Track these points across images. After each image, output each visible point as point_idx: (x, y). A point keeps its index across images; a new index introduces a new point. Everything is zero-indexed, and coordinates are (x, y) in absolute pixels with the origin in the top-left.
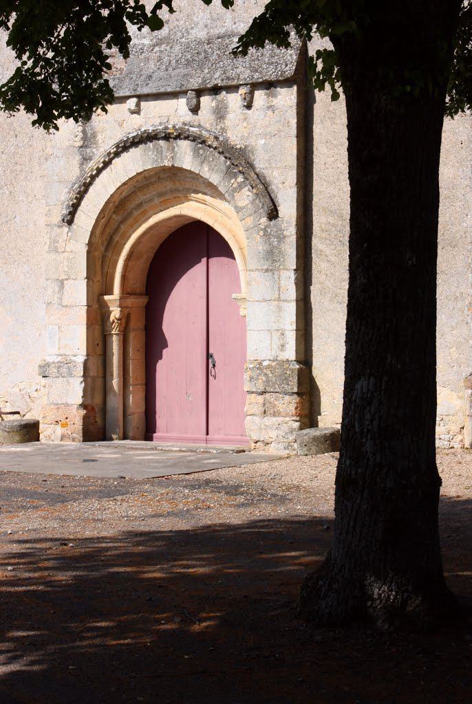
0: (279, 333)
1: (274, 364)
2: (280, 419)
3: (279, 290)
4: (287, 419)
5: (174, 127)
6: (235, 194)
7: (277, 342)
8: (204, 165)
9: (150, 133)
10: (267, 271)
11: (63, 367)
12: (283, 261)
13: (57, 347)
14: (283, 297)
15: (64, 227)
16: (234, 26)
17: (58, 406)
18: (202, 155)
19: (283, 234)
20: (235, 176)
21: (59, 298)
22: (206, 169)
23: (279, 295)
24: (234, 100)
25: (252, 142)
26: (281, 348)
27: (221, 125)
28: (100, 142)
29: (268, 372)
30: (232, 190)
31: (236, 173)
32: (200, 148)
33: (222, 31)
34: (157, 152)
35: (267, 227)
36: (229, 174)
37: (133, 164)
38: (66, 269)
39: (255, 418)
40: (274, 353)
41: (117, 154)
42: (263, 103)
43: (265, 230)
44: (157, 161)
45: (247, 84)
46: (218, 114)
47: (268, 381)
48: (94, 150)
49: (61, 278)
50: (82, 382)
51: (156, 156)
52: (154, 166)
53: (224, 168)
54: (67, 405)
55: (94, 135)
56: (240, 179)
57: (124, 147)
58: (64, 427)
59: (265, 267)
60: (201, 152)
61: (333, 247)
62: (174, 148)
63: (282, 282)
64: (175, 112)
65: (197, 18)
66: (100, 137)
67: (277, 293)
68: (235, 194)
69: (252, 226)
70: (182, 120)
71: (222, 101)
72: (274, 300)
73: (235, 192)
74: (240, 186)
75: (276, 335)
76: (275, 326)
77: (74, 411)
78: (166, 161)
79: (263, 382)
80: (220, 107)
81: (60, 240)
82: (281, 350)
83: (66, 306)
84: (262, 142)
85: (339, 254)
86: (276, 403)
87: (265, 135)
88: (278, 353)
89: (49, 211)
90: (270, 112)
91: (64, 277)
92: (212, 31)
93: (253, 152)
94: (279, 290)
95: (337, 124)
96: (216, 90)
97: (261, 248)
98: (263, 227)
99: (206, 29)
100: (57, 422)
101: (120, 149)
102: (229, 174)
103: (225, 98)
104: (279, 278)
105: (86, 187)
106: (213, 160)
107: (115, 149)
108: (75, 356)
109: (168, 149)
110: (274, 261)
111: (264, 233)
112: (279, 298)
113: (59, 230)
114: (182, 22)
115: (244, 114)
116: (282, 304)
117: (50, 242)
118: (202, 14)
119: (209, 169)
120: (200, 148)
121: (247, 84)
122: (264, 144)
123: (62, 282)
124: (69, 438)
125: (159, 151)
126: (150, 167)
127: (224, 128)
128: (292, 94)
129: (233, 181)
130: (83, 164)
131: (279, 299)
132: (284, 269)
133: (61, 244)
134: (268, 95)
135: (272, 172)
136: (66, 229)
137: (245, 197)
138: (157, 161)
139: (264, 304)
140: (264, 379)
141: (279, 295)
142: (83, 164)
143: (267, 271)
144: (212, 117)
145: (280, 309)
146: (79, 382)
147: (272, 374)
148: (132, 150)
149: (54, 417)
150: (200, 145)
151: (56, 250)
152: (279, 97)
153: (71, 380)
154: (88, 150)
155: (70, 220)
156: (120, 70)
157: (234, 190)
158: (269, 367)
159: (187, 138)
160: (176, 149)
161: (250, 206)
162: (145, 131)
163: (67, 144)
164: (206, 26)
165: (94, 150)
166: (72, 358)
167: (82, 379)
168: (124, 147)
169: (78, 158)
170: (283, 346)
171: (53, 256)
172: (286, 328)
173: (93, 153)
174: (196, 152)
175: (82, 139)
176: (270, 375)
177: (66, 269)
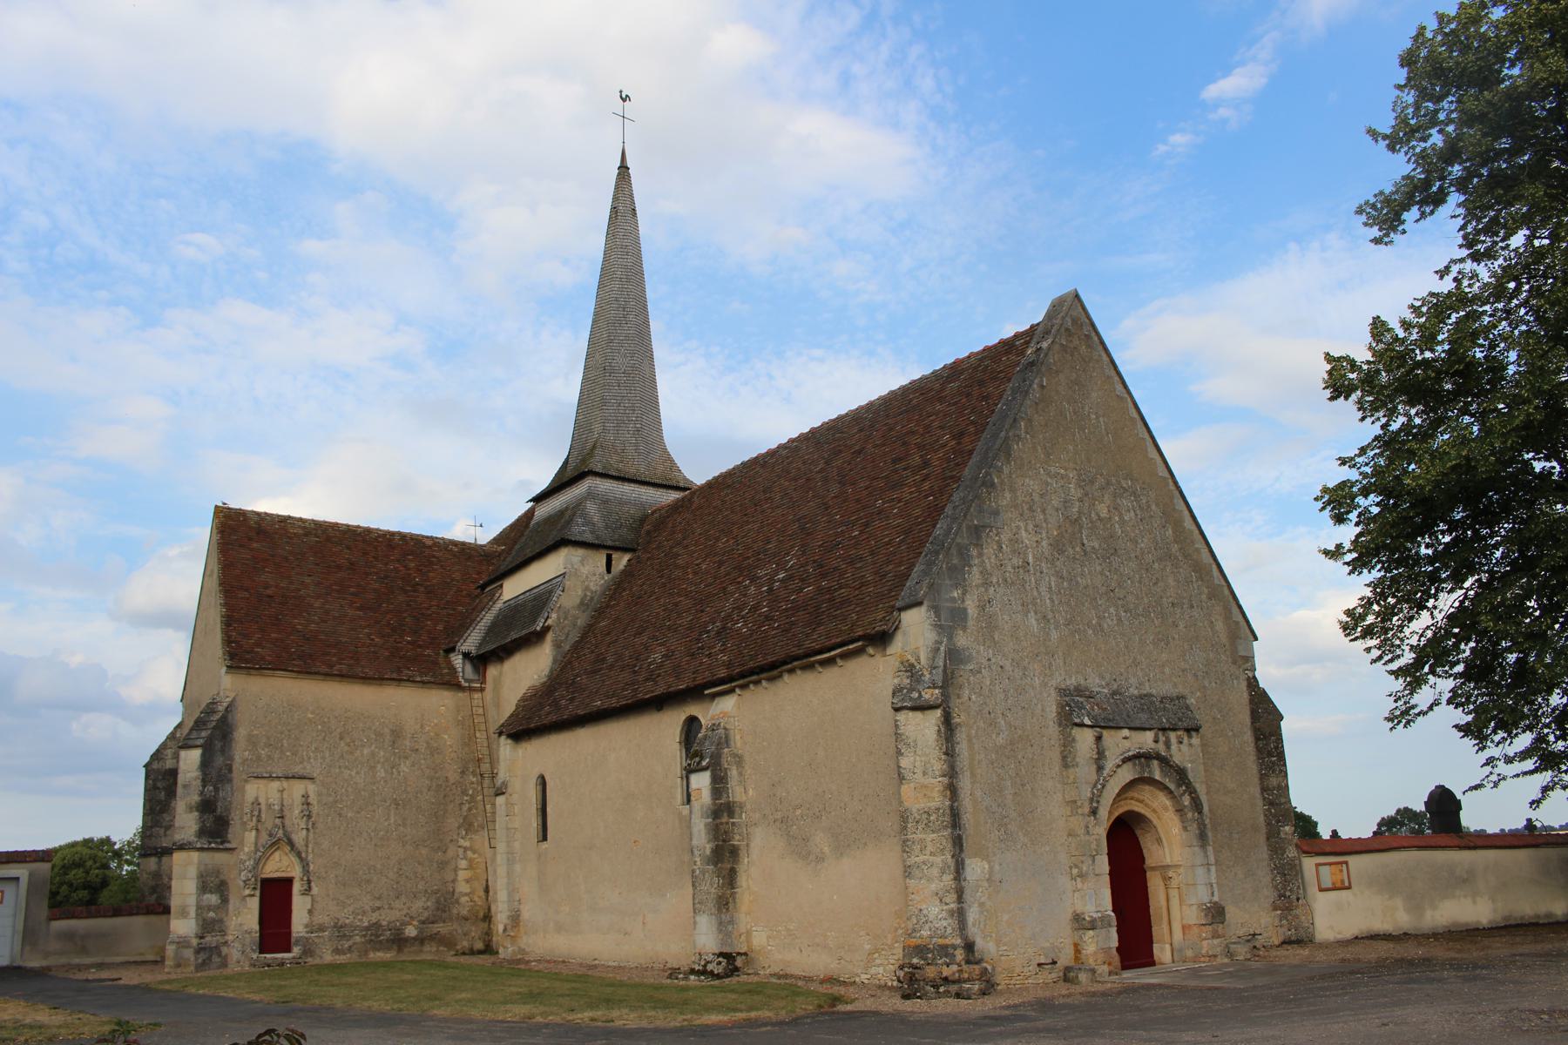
96: (1164, 730)
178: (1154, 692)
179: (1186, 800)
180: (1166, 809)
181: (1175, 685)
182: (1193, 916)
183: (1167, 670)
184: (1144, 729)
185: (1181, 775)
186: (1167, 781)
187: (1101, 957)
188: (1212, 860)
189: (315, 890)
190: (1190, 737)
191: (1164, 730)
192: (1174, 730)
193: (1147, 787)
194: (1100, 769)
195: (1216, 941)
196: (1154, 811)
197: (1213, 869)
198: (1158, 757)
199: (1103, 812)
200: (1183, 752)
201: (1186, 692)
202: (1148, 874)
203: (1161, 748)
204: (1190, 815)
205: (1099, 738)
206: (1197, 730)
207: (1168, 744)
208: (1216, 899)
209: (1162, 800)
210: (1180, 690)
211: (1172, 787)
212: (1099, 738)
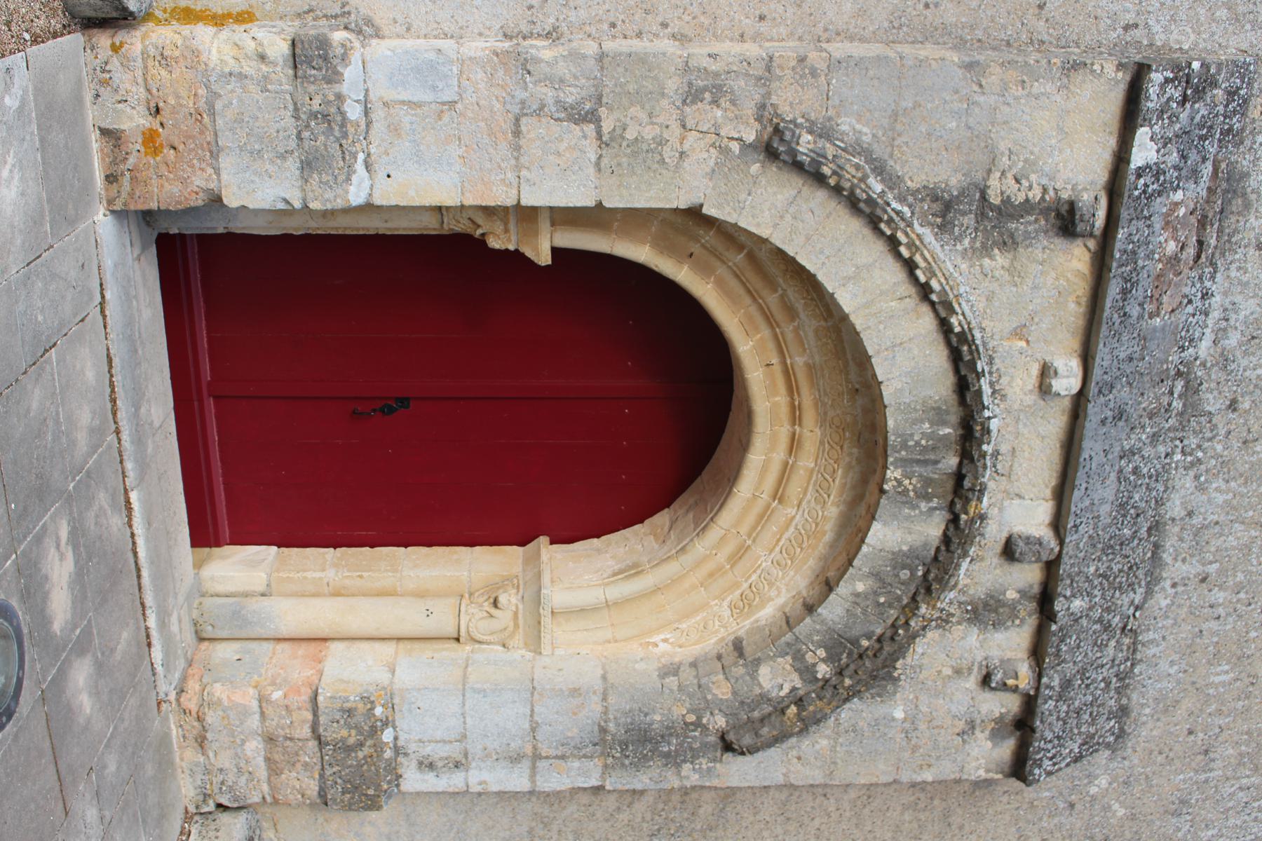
0: (460, 757)
1: (388, 754)
2: (262, 773)
3: (557, 757)
4: (265, 788)
5: (982, 517)
6: (789, 658)
7: (438, 752)
8: (870, 582)
9: (980, 446)
10: (603, 730)
11: (324, 132)
12: (623, 765)
13: (391, 95)
14: (541, 764)
15: (757, 126)
16: (1168, 584)
17: (204, 114)
18: (897, 576)
19: (684, 761)
20: (831, 658)
21: (542, 108)
22: (860, 587)
23: (547, 757)
24: (1010, 644)
25: (906, 692)
26: (426, 762)
27: (958, 613)
28: (986, 261)
29: (366, 750)
30: (799, 651)
31: (840, 660)
32: (913, 571)
33: (1167, 557)
34: (925, 449)
35: (705, 728)
36: (837, 645)
37: (908, 366)
38: (630, 134)
39: (257, 717)
40: (412, 747)
41: (944, 326)
42: (983, 712)
43: (698, 724)
44: (904, 445)
45: (1037, 689)
46: (986, 605)
47: (349, 749)
48: (966, 242)
49: (603, 112)
50: (287, 202)
51: (918, 443)
52: (891, 438)
53: (855, 632)
54: (215, 152)
55: (1009, 243)
56: (823, 670)
57: (961, 352)
58: (144, 143)
59: (611, 726)
60: (905, 574)
61: (648, 816)
62: (928, 497)
63: (576, 764)
64: (1017, 503)
65: (1216, 489)
66: (999, 260)
67: (553, 752)
68: (789, 658)
69: (709, 697)
70: (994, 512)
71: (1013, 615)
72: (535, 748)
73: (794, 659)
74: (807, 671)
75: (454, 751)
76: (475, 748)
77: (198, 181)
78: (898, 474)
79: (343, 740)
80: (1001, 610)
81: (719, 113)
82: (421, 763)
83: (517, 133)
84: (899, 714)
85: (633, 828)
86: (299, 766)
87: (911, 719)
88: (412, 756)
89: (814, 73)
90: (961, 725)
91: (607, 126)
92: (1177, 529)
93: (880, 695)
94: (557, 757)
95: (902, 814)
96: (1045, 600)
97: (657, 718)
98: (704, 721)
99: (1183, 513)
100: (158, 110)
101: (954, 340)
102: (837, 645)
103: (1017, 622)
104: (585, 756)
105: (870, 215)
106: (879, 604)
107: (957, 329)
108: (368, 166)
109: (928, 482)
110: (624, 745)
111: (692, 724)
112: (541, 758)
113: (749, 109)
114: (1219, 448)
115: (970, 669)
116: (526, 764)
117: (717, 75)
118: (1220, 498)
119: (858, 595)
120: (913, 571)
121: (1037, 689)
122: (893, 719)
123: (591, 117)
124: (114, 162)
125: (923, 457)
126: (891, 423)
127: (947, 622)
128: (988, 771)
129: (822, 653)
130: (936, 199)
131: (537, 756)
132: (606, 766)
133: (707, 115)
134: (1000, 720)
135: (828, 737)
136: (750, 137)
137: (780, 681)
138: (904, 445)
139: (527, 726)
140: (351, 741)
141: (547, 757)
142: (936, 199)
143: (603, 730)
144: (979, 592)
145: (516, 759)
146: (284, 195)
147: (365, 758)
148: (949, 380)
149: (172, 101)
150: (920, 573)
151: (692, 96)
152: (989, 744)
153: (292, 164)
154: (969, 220)
155: (775, 148)
156: (1179, 374)
157: (798, 657)
158: (379, 747)
159: (946, 540)
160: (924, 506)
161: (757, 691)
162: (989, 432)
163: (1003, 146)
164: (1190, 514)
165: (966, 242)
166: (361, 156)
167: (297, 205)
168: (961, 352)
169: (953, 182)
170: (431, 766)
171: (673, 85)
172: (471, 772)
173: (959, 239)
174: (901, 560)
175: (1007, 201)
176: (361, 754)
177: (630, 134)
178: (1161, 601)
179: (777, 678)
180: (745, 605)
181: (1166, 706)
182: (350, 672)
183: (1222, 675)
184: (1062, 493)
185: (867, 663)
186: (855, 584)
187: (175, 86)
188: (554, 780)
189: (519, 817)
190: (998, 730)
191: (1045, 600)
192: (1037, 653)
193: (833, 511)
194: (944, 209)
195: (254, 747)
196: (740, 553)
197: (518, 780)
198: (957, 536)
199: (773, 210)
200: (955, 674)
201: (1134, 755)
202: (514, 553)
203: (979, 573)
204: (722, 690)
205: (1066, 221)
206: (1019, 768)
207: (986, 612)
208: (413, 780)
209: (784, 588)
210: (1147, 729)
211: (834, 610)
212: (1066, 221)
